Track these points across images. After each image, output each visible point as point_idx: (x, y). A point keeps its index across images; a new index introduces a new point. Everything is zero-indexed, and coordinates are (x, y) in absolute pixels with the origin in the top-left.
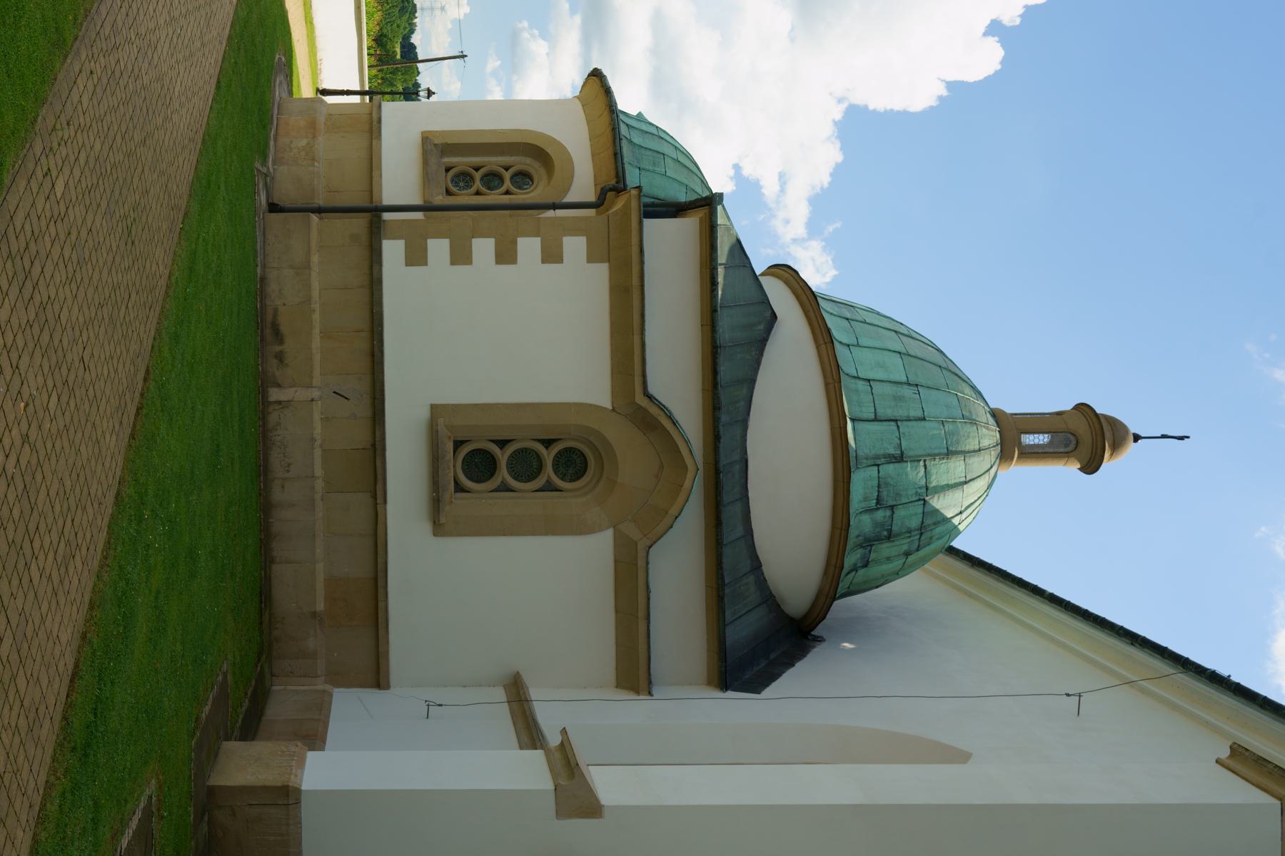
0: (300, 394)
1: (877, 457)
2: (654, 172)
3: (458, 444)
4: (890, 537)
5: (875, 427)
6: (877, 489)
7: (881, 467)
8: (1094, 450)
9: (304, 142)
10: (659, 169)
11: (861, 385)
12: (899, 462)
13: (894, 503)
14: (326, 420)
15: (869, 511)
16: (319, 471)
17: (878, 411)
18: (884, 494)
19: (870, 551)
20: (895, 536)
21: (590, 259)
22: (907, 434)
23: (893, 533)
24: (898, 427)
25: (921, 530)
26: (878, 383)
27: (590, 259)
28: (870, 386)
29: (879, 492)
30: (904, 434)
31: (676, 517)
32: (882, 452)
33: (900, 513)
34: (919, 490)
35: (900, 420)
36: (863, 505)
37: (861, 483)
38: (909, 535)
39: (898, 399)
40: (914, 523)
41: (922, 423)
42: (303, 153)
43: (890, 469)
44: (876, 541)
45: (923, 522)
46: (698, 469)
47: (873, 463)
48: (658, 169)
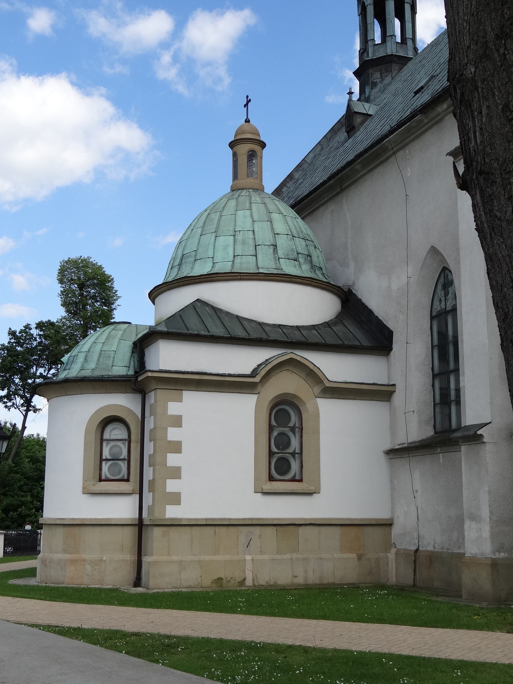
0: (249, 566)
1: (275, 258)
2: (114, 358)
3: (271, 479)
4: (309, 256)
5: (259, 256)
6: (290, 260)
7: (279, 257)
8: (252, 143)
9: (88, 567)
10: (112, 355)
11: (238, 260)
12: (277, 247)
13: (296, 252)
14: (262, 552)
15: (300, 265)
16: (288, 556)
17: (251, 254)
18: (292, 257)
19: (316, 266)
20: (309, 253)
21: (181, 401)
22: (262, 241)
23: (308, 254)
24: (259, 245)
25: (305, 240)
26: (236, 252)
27: (181, 401)
28: (237, 256)
29: (291, 259)
30: (262, 243)
31: (315, 365)
32: (272, 255)
33: (300, 251)
34: (289, 239)
35: (255, 243)
36: (298, 268)
37: (289, 268)
38: (308, 246)
39: (244, 243)
40: (303, 243)
41: (256, 232)
42: (96, 567)
43: (281, 252)
44: (312, 263)
45: (302, 238)
46: (292, 352)
47: (278, 261)
48: (112, 355)
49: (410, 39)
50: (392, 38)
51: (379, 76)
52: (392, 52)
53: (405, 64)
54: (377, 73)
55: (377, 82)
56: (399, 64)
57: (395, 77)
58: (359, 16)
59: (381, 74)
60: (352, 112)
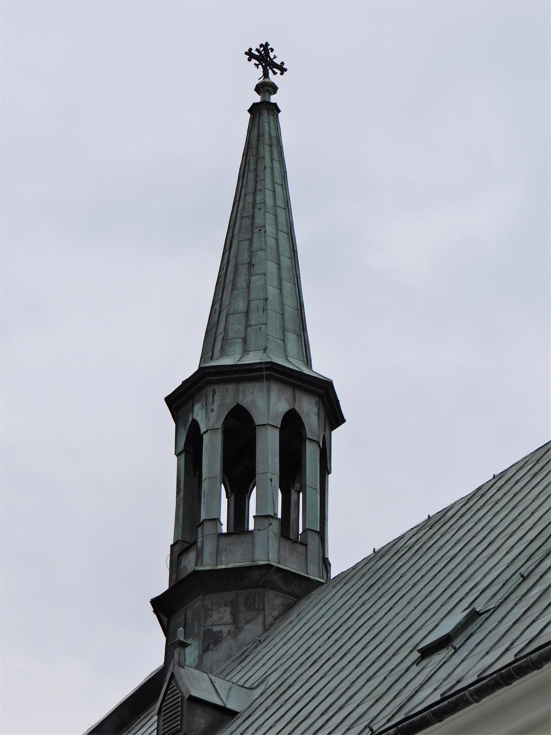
49: (314, 534)
50: (271, 524)
51: (228, 617)
52: (269, 560)
53: (298, 598)
54: (222, 609)
55: (220, 632)
56: (285, 592)
57: (271, 625)
58: (178, 455)
59: (234, 615)
60: (182, 698)
